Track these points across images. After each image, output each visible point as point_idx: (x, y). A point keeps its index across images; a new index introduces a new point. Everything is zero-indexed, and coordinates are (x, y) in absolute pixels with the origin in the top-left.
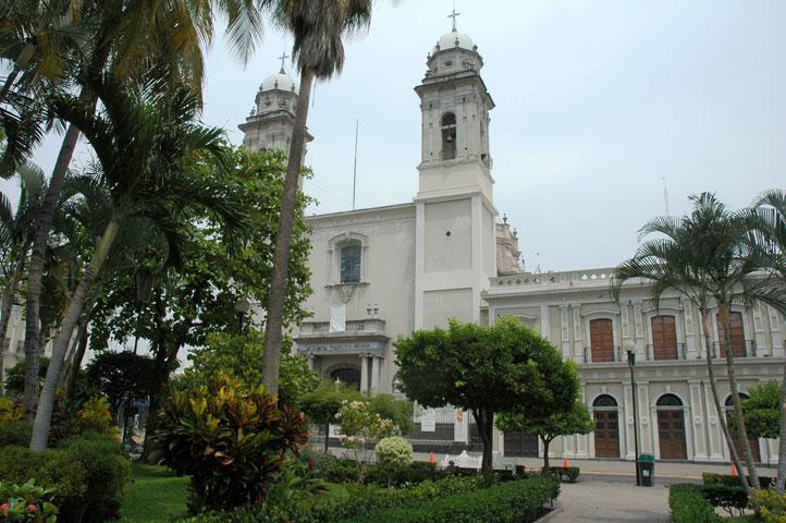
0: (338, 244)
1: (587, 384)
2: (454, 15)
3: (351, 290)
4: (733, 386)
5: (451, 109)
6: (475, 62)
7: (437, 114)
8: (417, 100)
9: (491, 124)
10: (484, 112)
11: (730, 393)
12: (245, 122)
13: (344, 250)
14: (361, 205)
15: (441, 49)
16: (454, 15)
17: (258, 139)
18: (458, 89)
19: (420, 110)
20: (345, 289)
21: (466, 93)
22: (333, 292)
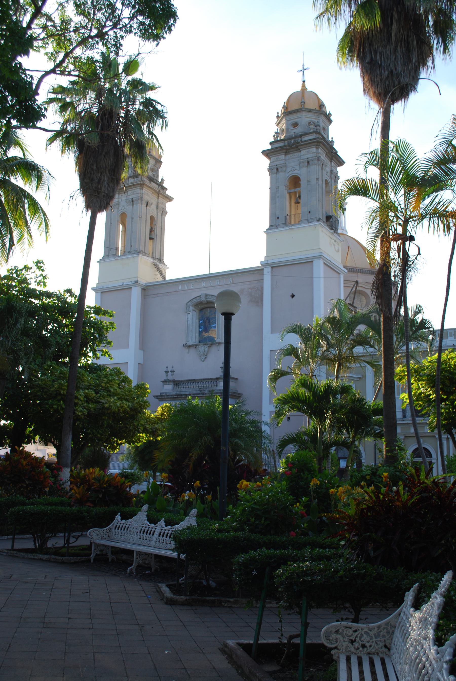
0: (196, 305)
1: (405, 437)
2: (303, 71)
3: (207, 349)
4: (419, 442)
5: (297, 173)
6: (322, 121)
7: (284, 176)
8: (266, 162)
9: (168, 218)
10: (332, 171)
11: (416, 446)
12: (269, 147)
13: (201, 310)
14: (215, 269)
15: (289, 110)
16: (303, 71)
17: (285, 166)
18: (303, 152)
19: (268, 173)
20: (202, 348)
21: (309, 156)
22: (192, 350)
